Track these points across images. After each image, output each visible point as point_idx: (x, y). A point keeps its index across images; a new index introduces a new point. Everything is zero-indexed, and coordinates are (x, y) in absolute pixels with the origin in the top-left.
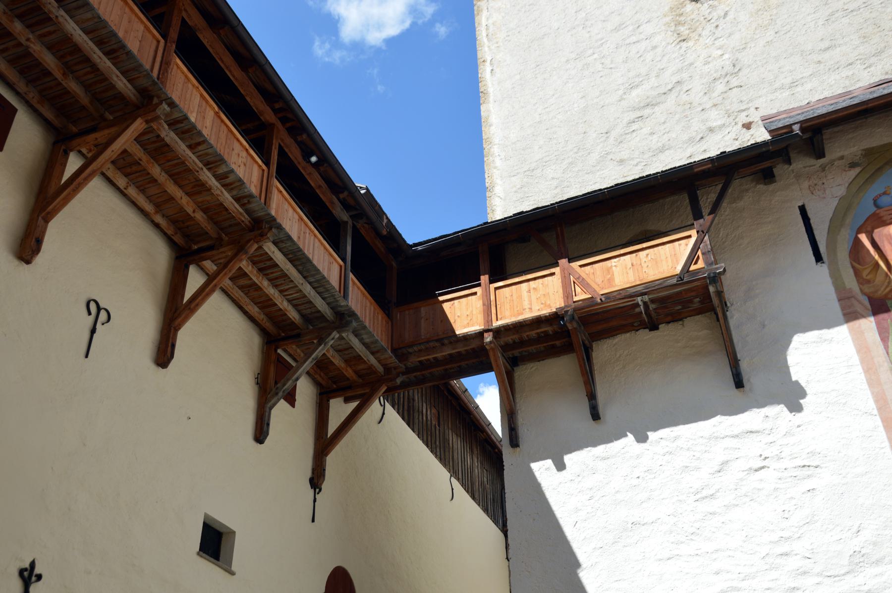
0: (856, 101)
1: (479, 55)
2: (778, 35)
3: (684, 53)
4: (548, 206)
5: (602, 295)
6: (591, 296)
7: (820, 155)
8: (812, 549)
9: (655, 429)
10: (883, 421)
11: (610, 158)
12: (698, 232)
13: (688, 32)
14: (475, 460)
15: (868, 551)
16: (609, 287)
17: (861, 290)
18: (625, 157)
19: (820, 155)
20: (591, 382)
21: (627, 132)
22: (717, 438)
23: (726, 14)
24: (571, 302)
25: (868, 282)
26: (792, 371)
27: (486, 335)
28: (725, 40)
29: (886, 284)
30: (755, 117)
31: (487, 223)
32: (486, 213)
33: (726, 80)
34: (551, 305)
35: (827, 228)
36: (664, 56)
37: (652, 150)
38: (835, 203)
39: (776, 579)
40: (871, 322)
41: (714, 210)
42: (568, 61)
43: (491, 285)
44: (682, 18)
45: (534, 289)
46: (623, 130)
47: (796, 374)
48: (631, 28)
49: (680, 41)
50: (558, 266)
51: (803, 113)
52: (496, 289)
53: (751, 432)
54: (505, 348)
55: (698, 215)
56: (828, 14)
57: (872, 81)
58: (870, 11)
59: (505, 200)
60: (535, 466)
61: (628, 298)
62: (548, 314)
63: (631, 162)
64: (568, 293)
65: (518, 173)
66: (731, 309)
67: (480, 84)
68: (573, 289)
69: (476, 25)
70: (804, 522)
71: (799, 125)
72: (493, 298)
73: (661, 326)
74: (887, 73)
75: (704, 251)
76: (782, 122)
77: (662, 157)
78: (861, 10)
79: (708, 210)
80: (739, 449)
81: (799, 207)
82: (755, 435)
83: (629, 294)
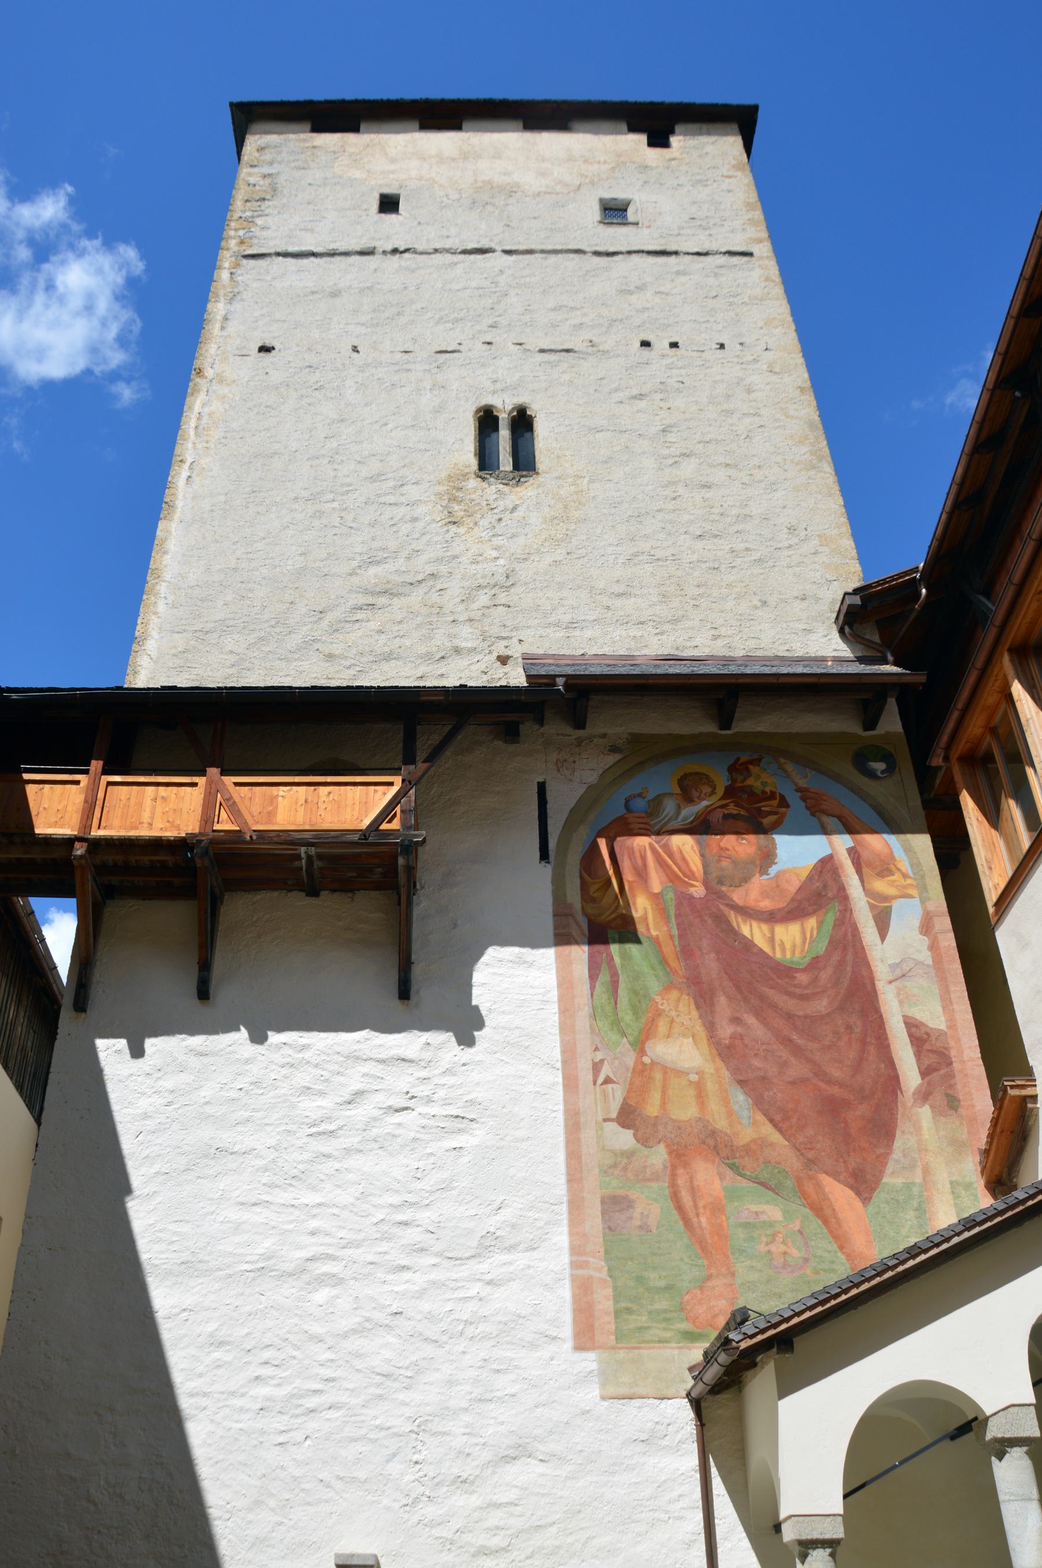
0: (636, 671)
1: (178, 450)
2: (569, 557)
3: (450, 540)
4: (213, 689)
5: (254, 831)
6: (238, 828)
7: (580, 725)
8: (439, 1222)
9: (280, 1030)
10: (564, 1078)
11: (316, 648)
12: (403, 781)
13: (462, 513)
14: (22, 1014)
15: (503, 1234)
16: (266, 823)
17: (583, 908)
18: (336, 653)
19: (580, 725)
20: (209, 945)
21: (347, 619)
22: (358, 1058)
23: (514, 509)
24: (208, 830)
25: (594, 900)
26: (475, 992)
27: (77, 845)
28: (505, 541)
29: (613, 908)
30: (516, 651)
31: (121, 688)
32: (124, 674)
33: (493, 592)
34: (181, 827)
35: (565, 819)
36: (423, 534)
37: (374, 654)
38: (581, 790)
39: (385, 1253)
40: (583, 951)
41: (430, 759)
42: (296, 498)
43: (103, 777)
44: (460, 494)
45: (163, 798)
46: (343, 615)
47: (480, 997)
48: (391, 483)
49: (450, 522)
50: (204, 775)
51: (573, 665)
52: (109, 784)
53: (404, 1060)
54: (101, 870)
55: (409, 758)
56: (631, 552)
57: (660, 653)
58: (678, 566)
59: (156, 662)
60: (100, 1043)
61: (289, 844)
62: (172, 839)
63: (343, 662)
64: (208, 816)
65: (185, 631)
66: (420, 893)
67: (167, 490)
68: (217, 813)
69: (186, 408)
70: (439, 1187)
71: (564, 679)
72: (101, 795)
73: (324, 894)
74: (677, 649)
75: (404, 808)
76: (546, 668)
77: (385, 666)
78: (668, 562)
79: (425, 755)
80: (382, 1078)
81: (538, 783)
82: (407, 1064)
83: (289, 840)
